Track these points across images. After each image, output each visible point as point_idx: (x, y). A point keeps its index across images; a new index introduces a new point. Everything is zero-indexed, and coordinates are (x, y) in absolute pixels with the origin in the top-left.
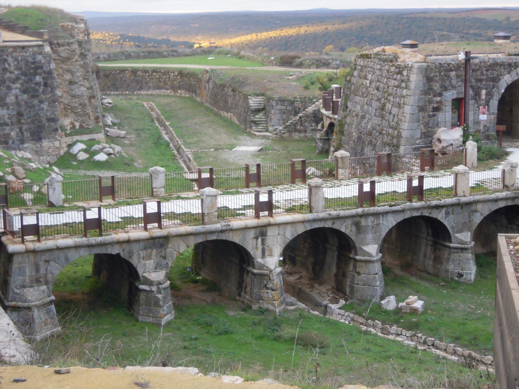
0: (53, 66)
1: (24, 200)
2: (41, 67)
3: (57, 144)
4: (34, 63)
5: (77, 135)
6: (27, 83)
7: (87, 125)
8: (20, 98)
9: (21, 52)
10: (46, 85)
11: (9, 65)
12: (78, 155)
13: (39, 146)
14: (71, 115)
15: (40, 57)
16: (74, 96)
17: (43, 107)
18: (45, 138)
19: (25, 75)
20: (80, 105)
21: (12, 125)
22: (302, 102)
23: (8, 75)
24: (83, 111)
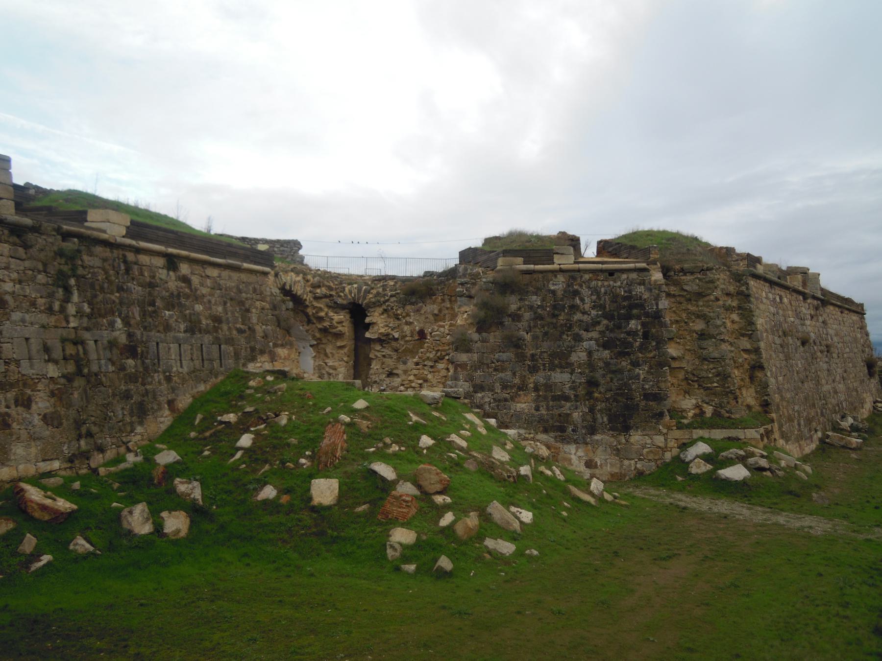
0: (664, 303)
2: (641, 306)
3: (659, 440)
4: (625, 298)
5: (701, 428)
6: (612, 331)
7: (727, 412)
8: (596, 356)
9: (606, 280)
10: (646, 336)
11: (582, 300)
13: (623, 441)
14: (698, 391)
15: (640, 289)
17: (639, 375)
18: (637, 428)
19: (609, 316)
20: (717, 376)
21: (577, 401)
23: (578, 316)
24: (723, 386)
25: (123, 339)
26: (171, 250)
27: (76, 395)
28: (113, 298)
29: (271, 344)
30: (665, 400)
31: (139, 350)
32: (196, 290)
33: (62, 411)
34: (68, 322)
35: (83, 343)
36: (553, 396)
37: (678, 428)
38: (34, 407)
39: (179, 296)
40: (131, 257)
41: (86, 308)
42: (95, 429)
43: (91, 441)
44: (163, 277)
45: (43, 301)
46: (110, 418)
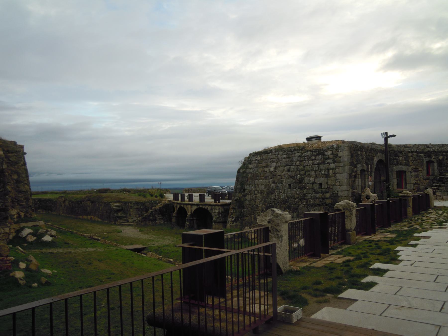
1: (16, 279)
3: (7, 230)
7: (30, 215)
12: (28, 238)
16: (20, 192)
20: (25, 199)
22: (150, 203)
30: (8, 211)
37: (15, 223)
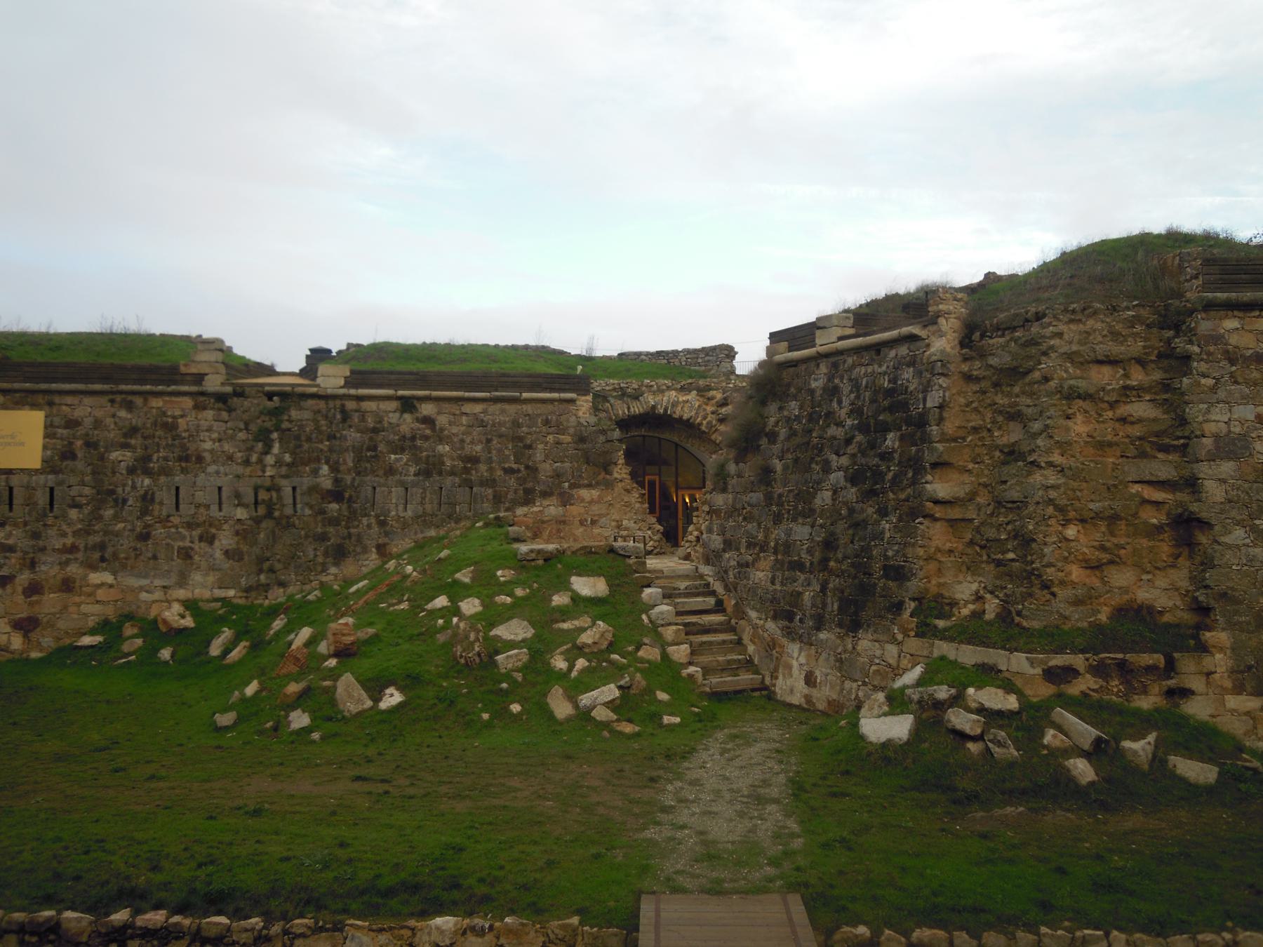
15: (908, 374)
20: (1015, 537)
25: (327, 484)
26: (400, 393)
27: (262, 535)
28: (321, 446)
29: (567, 484)
31: (347, 495)
32: (442, 430)
33: (245, 548)
34: (264, 472)
35: (278, 490)
36: (790, 562)
38: (217, 543)
39: (413, 438)
40: (351, 405)
41: (287, 458)
42: (278, 566)
43: (273, 576)
44: (394, 421)
45: (239, 455)
46: (299, 557)
